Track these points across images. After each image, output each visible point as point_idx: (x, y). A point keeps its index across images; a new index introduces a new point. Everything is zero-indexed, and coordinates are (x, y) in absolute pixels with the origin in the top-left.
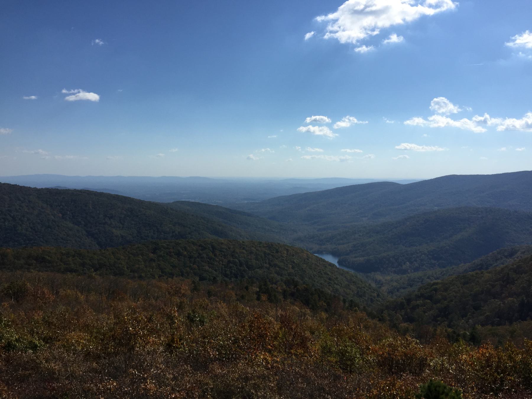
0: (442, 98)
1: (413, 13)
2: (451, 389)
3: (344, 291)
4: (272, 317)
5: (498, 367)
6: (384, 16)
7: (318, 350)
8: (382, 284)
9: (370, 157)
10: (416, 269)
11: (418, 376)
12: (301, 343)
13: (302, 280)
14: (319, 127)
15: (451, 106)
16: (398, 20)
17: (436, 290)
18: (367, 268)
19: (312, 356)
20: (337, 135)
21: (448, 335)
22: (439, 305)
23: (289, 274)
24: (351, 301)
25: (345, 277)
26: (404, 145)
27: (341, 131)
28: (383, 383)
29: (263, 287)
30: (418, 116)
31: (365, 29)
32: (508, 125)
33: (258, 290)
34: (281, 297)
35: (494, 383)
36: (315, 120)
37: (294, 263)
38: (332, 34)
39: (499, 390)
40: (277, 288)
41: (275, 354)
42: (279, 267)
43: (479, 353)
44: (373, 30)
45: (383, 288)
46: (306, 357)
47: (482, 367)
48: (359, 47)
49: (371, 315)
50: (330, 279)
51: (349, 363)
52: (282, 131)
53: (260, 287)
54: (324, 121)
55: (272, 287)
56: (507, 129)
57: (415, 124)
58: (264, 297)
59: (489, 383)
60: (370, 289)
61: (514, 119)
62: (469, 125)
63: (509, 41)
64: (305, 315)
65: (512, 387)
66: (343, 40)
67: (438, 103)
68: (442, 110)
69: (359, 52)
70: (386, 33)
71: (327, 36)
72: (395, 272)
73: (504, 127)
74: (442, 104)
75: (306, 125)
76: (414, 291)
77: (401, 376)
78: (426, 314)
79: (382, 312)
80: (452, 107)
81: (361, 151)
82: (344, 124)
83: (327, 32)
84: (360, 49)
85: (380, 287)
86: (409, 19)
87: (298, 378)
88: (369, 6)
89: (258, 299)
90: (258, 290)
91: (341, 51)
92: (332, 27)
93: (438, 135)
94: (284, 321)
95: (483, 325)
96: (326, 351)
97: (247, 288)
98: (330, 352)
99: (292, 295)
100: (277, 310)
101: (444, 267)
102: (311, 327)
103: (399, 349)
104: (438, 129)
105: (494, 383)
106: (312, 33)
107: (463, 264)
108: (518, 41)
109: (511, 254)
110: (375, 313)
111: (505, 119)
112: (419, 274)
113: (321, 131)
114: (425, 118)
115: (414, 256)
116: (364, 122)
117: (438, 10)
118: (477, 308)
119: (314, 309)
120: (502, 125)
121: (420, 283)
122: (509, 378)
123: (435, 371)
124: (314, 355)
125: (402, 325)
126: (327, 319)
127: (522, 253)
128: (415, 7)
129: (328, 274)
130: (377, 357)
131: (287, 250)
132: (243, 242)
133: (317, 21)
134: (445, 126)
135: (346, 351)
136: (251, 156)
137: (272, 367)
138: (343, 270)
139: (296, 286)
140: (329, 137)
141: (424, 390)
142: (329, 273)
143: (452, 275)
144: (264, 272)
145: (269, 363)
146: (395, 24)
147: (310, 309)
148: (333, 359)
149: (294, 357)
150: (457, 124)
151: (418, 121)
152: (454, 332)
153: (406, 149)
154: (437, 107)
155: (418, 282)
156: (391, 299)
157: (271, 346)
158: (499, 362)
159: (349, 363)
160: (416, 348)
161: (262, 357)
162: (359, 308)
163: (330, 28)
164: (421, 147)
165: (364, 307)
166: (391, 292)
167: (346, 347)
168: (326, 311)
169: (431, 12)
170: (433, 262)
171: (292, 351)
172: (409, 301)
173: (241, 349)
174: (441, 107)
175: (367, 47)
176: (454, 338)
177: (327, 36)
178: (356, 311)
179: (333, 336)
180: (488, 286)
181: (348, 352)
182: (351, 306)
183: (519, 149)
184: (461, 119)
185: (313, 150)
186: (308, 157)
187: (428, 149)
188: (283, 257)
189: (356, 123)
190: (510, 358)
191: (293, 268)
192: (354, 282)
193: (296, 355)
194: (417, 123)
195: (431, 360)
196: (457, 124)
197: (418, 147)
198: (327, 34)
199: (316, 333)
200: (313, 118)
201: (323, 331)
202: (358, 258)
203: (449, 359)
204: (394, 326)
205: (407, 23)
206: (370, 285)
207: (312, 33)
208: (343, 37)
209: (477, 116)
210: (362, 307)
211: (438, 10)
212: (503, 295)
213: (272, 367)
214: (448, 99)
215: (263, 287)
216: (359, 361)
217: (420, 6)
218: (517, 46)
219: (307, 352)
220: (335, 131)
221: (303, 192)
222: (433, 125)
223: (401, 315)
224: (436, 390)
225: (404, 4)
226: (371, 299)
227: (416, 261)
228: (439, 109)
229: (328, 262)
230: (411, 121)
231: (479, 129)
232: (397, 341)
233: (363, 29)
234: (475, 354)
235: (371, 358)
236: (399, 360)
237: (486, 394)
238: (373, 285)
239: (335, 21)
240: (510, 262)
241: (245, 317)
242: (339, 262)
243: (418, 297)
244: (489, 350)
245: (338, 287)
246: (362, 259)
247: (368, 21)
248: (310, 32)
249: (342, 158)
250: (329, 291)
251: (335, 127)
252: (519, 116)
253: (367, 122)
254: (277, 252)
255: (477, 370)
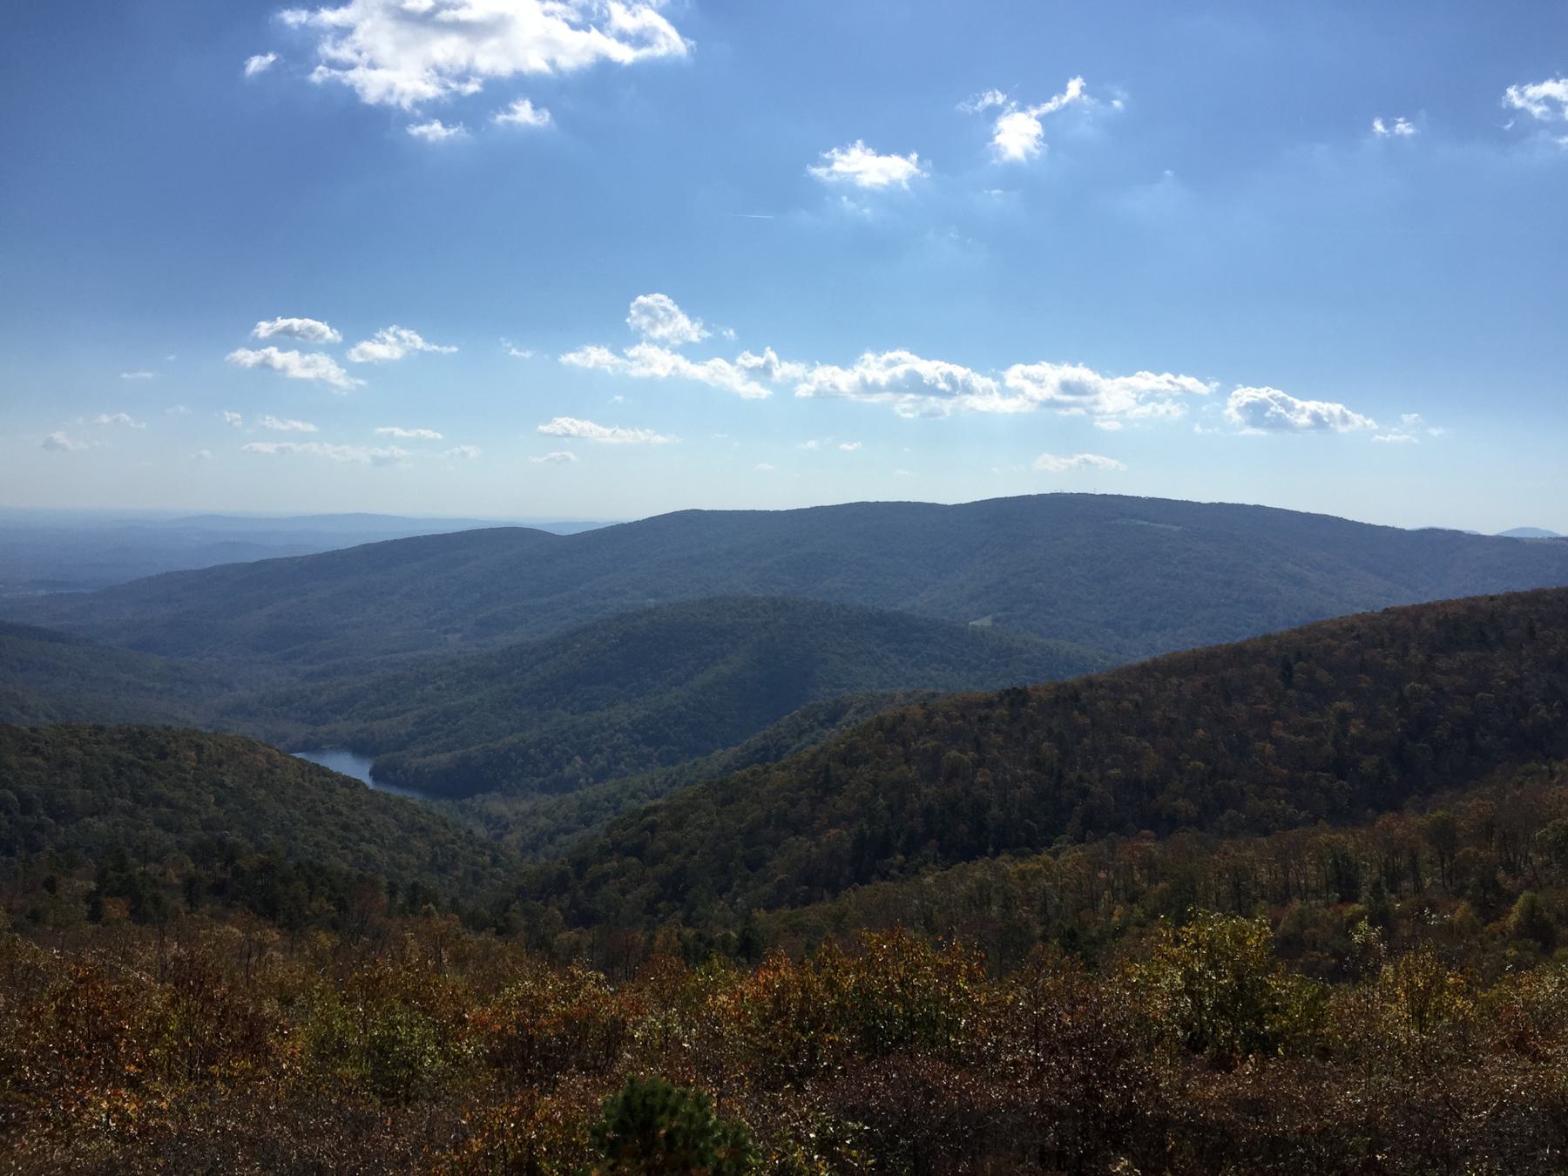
0: (658, 296)
1: (579, 48)
2: (684, 1095)
3: (392, 858)
4: (143, 971)
5: (802, 1013)
6: (493, 42)
7: (302, 1052)
8: (506, 827)
9: (464, 454)
10: (601, 776)
11: (601, 1074)
12: (246, 1038)
13: (251, 840)
14: (299, 353)
15: (683, 322)
16: (536, 62)
17: (652, 828)
18: (461, 782)
19: (283, 1073)
20: (361, 382)
21: (685, 947)
22: (661, 868)
23: (207, 826)
24: (415, 886)
25: (395, 817)
26: (564, 423)
27: (369, 369)
28: (501, 1115)
29: (111, 874)
30: (598, 342)
31: (440, 72)
32: (820, 383)
33: (93, 886)
34: (178, 902)
35: (795, 1058)
36: (288, 331)
37: (223, 785)
38: (334, 72)
39: (806, 1073)
40: (163, 874)
41: (156, 1086)
42: (169, 805)
43: (758, 984)
44: (463, 77)
45: (508, 838)
46: (261, 1079)
47: (765, 1021)
48: (420, 122)
49: (475, 922)
50: (345, 827)
51: (404, 1073)
52: (171, 358)
53: (101, 878)
54: (321, 335)
55: (143, 874)
56: (818, 393)
57: (590, 365)
58: (115, 909)
59: (783, 1060)
60: (471, 843)
61: (836, 369)
62: (727, 375)
63: (818, 162)
64: (262, 947)
65: (837, 1061)
66: (371, 96)
67: (647, 310)
68: (660, 331)
69: (423, 137)
70: (501, 91)
71: (319, 75)
72: (543, 789)
73: (812, 388)
74: (662, 314)
75: (258, 344)
76: (596, 836)
77: (556, 1082)
78: (629, 897)
79: (506, 909)
80: (684, 326)
81: (439, 436)
82: (384, 348)
83: (319, 63)
84: (424, 129)
85: (500, 837)
86: (567, 62)
87: (234, 1151)
88: (448, 7)
89: (95, 916)
90: (93, 886)
91: (366, 127)
92: (335, 47)
93: (654, 401)
94: (188, 979)
95: (769, 908)
96: (329, 1049)
97: (51, 885)
98: (342, 1051)
99: (219, 889)
100: (162, 945)
101: (673, 762)
102: (281, 984)
103: (551, 1007)
104: (652, 381)
105: (795, 1058)
106: (271, 58)
107: (720, 751)
108: (837, 167)
109: (833, 718)
110: (487, 913)
111: (813, 365)
112: (611, 786)
113: (308, 366)
114: (617, 351)
115: (594, 737)
116: (445, 350)
117: (644, 52)
118: (754, 865)
119: (294, 925)
120: (806, 380)
121: (610, 814)
122: (828, 1037)
123: (647, 1055)
124: (290, 1068)
125: (564, 936)
126: (335, 951)
127: (858, 712)
128: (583, 33)
129: (340, 814)
130: (489, 1042)
131: (199, 748)
132: (33, 730)
133: (283, 26)
134: (670, 376)
135: (395, 1041)
136: (59, 436)
137: (144, 1131)
138: (387, 796)
139: (230, 860)
140: (337, 387)
141: (614, 1112)
142: (345, 810)
143: (693, 783)
144: (116, 824)
145: (130, 1121)
146: (525, 70)
147: (280, 927)
148: (350, 1072)
149: (219, 1086)
150: (699, 372)
151: (596, 356)
152: (700, 937)
153: (568, 435)
154: (645, 320)
155: (606, 810)
156: (533, 867)
157: (139, 1066)
158: (805, 999)
159: (404, 1073)
160: (596, 997)
161: (104, 1105)
162: (437, 905)
163: (327, 50)
164: (608, 431)
165: (454, 901)
166: (531, 847)
167: (394, 1027)
168: (334, 926)
169: (624, 54)
170: (645, 750)
171: (214, 1069)
172: (581, 866)
173: (27, 1092)
174: (656, 321)
175: (445, 125)
176: (695, 954)
177: (319, 75)
178: (428, 914)
179: (348, 1000)
180: (781, 803)
181: (401, 1042)
182: (412, 901)
183: (845, 446)
184: (709, 359)
185: (283, 427)
186: (268, 448)
187: (626, 436)
188: (185, 771)
189: (421, 351)
190: (831, 985)
191: (219, 802)
192: (421, 829)
193: (224, 1079)
194: (597, 362)
195: (636, 1025)
196: (699, 372)
197: (601, 429)
198: (320, 68)
199: (300, 999)
200: (282, 323)
201: (322, 992)
202: (435, 757)
203: (682, 1015)
204: (541, 945)
205: (560, 72)
206: (470, 832)
207: (271, 58)
208: (372, 84)
209: (747, 353)
210: (445, 901)
211: (644, 52)
212: (816, 824)
213: (144, 1131)
214: (676, 303)
215: (111, 874)
216: (434, 1062)
217: (594, 31)
218: (835, 178)
219: (267, 1064)
220: (354, 370)
221: (254, 558)
222: (639, 372)
223: (561, 909)
224: (644, 1104)
225: (550, 20)
226: (475, 874)
227: (599, 751)
228: (652, 326)
229: (339, 774)
230: (580, 355)
231: (754, 390)
232: (544, 983)
233: (432, 72)
234: (749, 989)
235: (469, 1046)
236: (549, 1039)
237: (774, 1090)
238: (481, 832)
239: (344, 32)
240: (831, 736)
241: (43, 985)
242: (374, 774)
243: (606, 852)
244: (783, 972)
245: (373, 849)
246: (444, 758)
247: (447, 49)
248: (265, 54)
249: (381, 453)
250: (345, 866)
251: (354, 356)
252: (846, 362)
253: (454, 349)
254: (163, 755)
255: (750, 1030)
